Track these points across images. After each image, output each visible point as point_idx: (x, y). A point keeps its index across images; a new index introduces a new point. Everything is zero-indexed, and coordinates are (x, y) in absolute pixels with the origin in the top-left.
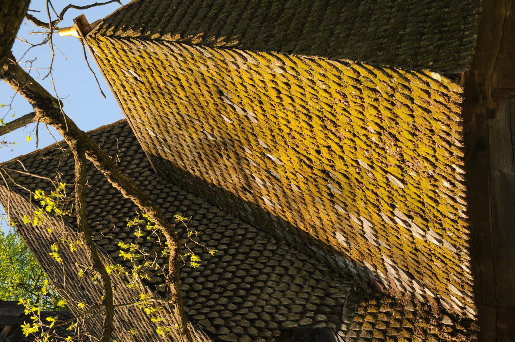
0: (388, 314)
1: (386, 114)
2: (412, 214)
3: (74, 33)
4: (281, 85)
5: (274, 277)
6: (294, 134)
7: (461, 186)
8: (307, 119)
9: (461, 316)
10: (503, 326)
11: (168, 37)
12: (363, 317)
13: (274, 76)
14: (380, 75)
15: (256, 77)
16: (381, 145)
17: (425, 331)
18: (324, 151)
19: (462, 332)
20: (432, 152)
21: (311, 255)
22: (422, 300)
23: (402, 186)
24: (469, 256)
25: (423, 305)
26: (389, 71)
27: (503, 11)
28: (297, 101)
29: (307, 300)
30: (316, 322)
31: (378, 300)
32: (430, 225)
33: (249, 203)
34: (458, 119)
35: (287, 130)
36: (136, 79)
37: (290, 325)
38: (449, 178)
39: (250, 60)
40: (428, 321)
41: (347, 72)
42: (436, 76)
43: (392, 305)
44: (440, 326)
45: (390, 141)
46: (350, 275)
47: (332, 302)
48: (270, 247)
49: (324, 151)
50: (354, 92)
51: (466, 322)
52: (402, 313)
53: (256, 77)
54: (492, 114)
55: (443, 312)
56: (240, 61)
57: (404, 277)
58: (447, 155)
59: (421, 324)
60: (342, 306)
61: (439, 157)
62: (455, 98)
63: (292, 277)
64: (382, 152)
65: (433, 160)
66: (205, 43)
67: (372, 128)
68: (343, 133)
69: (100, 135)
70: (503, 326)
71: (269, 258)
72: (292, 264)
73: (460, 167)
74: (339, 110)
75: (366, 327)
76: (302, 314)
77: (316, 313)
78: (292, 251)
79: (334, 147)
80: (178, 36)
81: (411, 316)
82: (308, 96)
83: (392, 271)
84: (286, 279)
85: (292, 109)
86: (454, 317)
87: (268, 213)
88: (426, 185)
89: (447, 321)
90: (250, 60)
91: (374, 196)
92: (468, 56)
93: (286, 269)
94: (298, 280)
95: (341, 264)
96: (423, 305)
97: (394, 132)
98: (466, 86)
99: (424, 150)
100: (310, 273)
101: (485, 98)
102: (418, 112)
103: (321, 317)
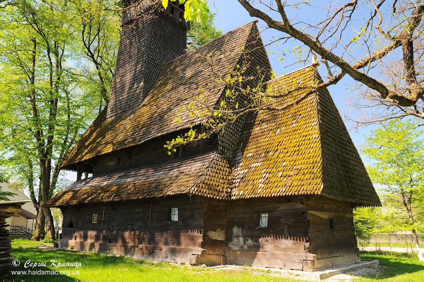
0: (226, 171)
1: (306, 171)
2: (268, 179)
3: (314, 62)
4: (309, 137)
5: (231, 131)
6: (290, 140)
7: (284, 194)
8: (297, 145)
9: (231, 195)
10: (222, 208)
11: (318, 98)
12: (224, 162)
13: (306, 136)
14: (319, 170)
15: (310, 128)
16: (294, 169)
17: (224, 183)
18: (286, 150)
19: (227, 195)
20: (295, 185)
21: (239, 144)
22: (234, 182)
23: (280, 176)
24: (250, 198)
25: (232, 182)
26: (321, 172)
27: (326, 206)
28: (304, 142)
29: (226, 143)
30: (220, 146)
31: (230, 167)
32: (266, 185)
33: (254, 122)
34: (309, 193)
35: (291, 138)
36: (299, 83)
37: (218, 137)
38: (286, 191)
39: (316, 127)
40: (228, 184)
41: (318, 159)
42: (322, 187)
43: (229, 172)
44: (227, 188)
45: (296, 172)
46: (235, 157)
47: (226, 151)
48: (240, 129)
49: (286, 150)
50: (312, 162)
51: (230, 196)
52: (228, 176)
53: (310, 128)
54: (302, 203)
55: (231, 189)
56: (315, 123)
57: (242, 176)
58: (295, 190)
59: (226, 182)
60: (225, 155)
61: (294, 188)
62: (287, 194)
63: (232, 138)
64: (291, 170)
65: (292, 185)
66: (319, 111)
67: (299, 167)
68: (295, 157)
69: (268, 64)
70: (222, 208)
71: (236, 129)
72: (235, 137)
73: (291, 194)
74: (304, 156)
75: (221, 164)
76: (222, 141)
77: (222, 146)
78: (239, 137)
79: (289, 154)
80: (319, 101)
81: (227, 178)
82: (307, 146)
83: (242, 172)
84: (231, 135)
85: (300, 140)
86: (230, 192)
87: (252, 129)
88: (282, 184)
89: (229, 190)
90: (316, 127)
91: (272, 167)
92: (327, 196)
93: (234, 135)
94: (231, 139)
95: (238, 155)
96: (232, 182)
97: (299, 174)
98: (321, 196)
99: (295, 183)
100: (233, 144)
101: (307, 201)
102: (309, 181)
103: (221, 148)
